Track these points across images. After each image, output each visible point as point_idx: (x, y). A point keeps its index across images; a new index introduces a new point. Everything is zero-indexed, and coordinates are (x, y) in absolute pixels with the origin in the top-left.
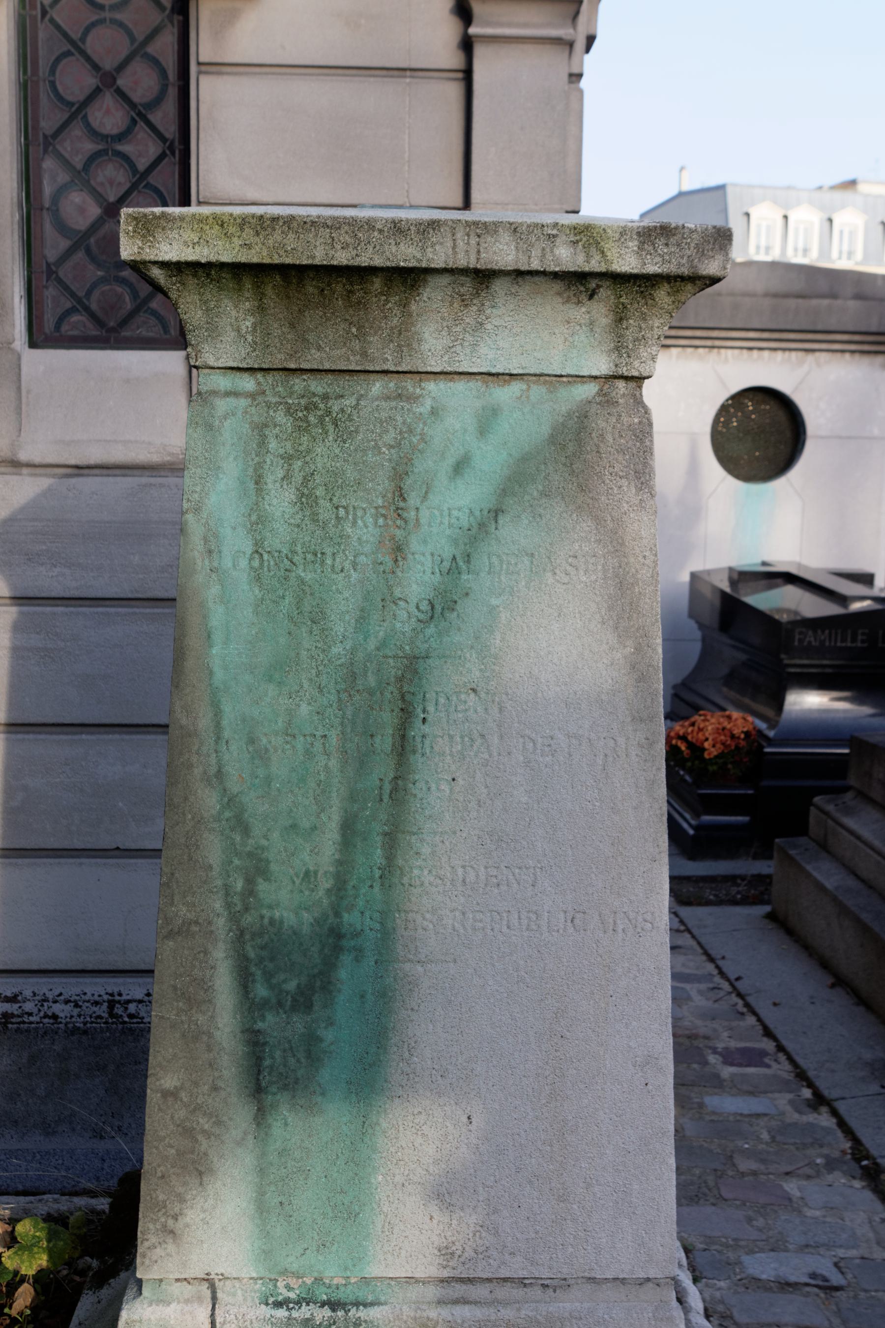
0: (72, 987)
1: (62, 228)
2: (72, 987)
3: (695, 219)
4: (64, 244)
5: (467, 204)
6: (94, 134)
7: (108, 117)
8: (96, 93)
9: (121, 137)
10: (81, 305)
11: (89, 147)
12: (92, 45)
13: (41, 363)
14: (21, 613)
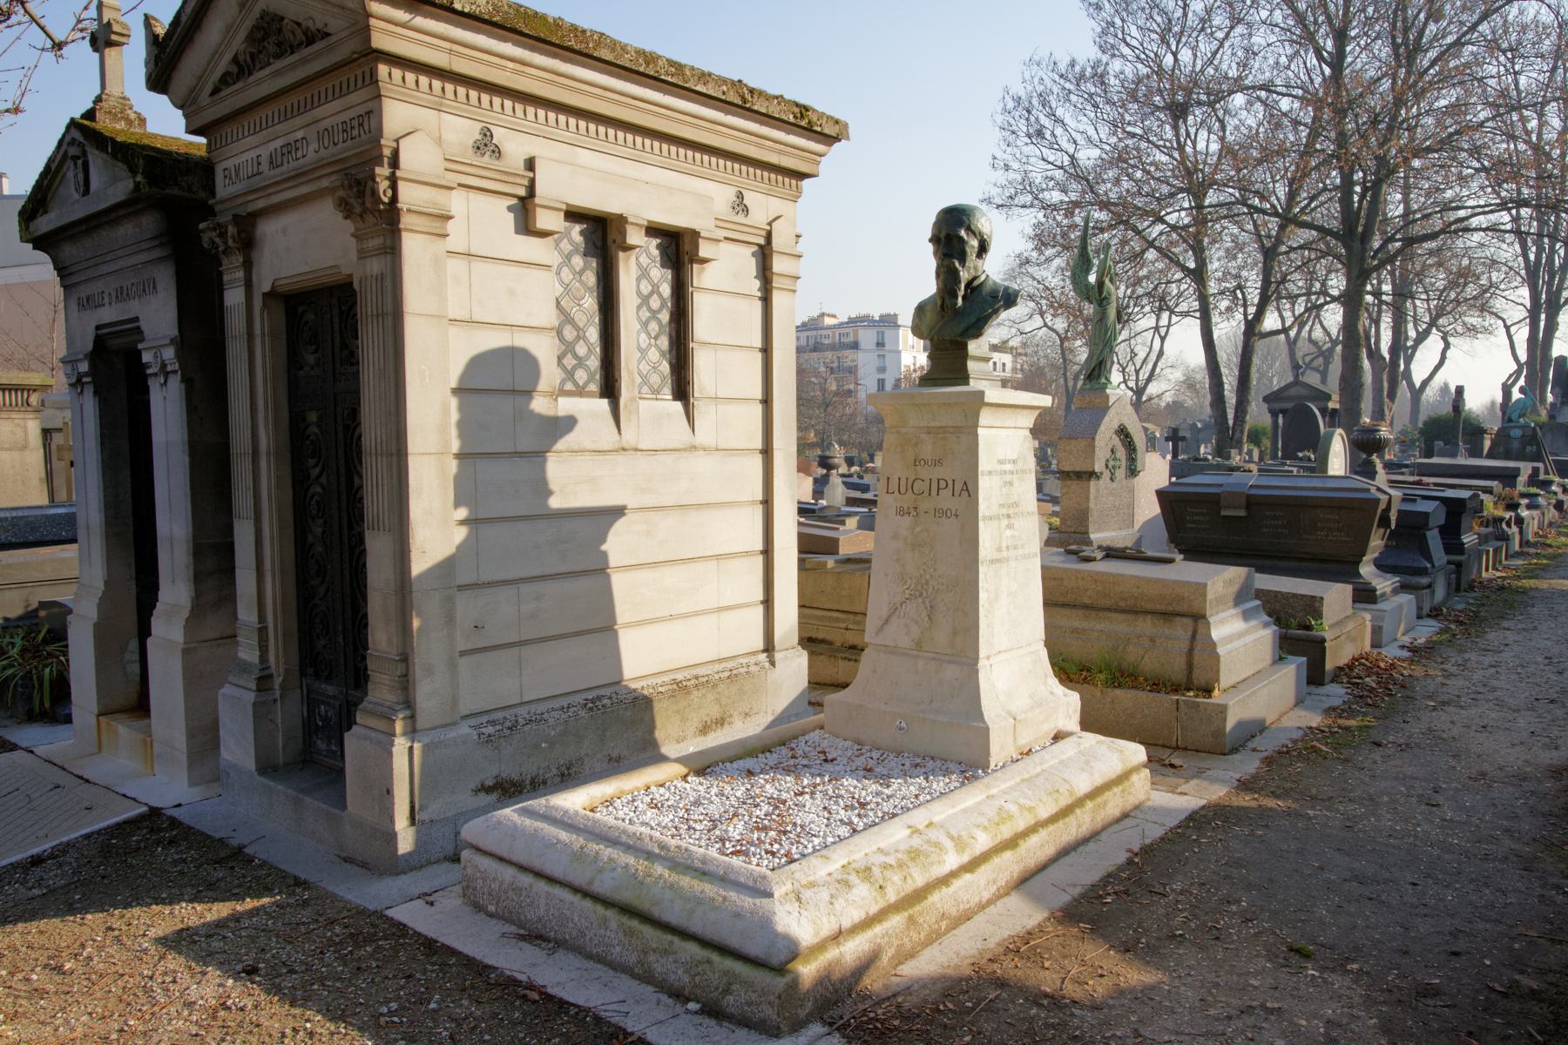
0: (718, 667)
2: (718, 667)
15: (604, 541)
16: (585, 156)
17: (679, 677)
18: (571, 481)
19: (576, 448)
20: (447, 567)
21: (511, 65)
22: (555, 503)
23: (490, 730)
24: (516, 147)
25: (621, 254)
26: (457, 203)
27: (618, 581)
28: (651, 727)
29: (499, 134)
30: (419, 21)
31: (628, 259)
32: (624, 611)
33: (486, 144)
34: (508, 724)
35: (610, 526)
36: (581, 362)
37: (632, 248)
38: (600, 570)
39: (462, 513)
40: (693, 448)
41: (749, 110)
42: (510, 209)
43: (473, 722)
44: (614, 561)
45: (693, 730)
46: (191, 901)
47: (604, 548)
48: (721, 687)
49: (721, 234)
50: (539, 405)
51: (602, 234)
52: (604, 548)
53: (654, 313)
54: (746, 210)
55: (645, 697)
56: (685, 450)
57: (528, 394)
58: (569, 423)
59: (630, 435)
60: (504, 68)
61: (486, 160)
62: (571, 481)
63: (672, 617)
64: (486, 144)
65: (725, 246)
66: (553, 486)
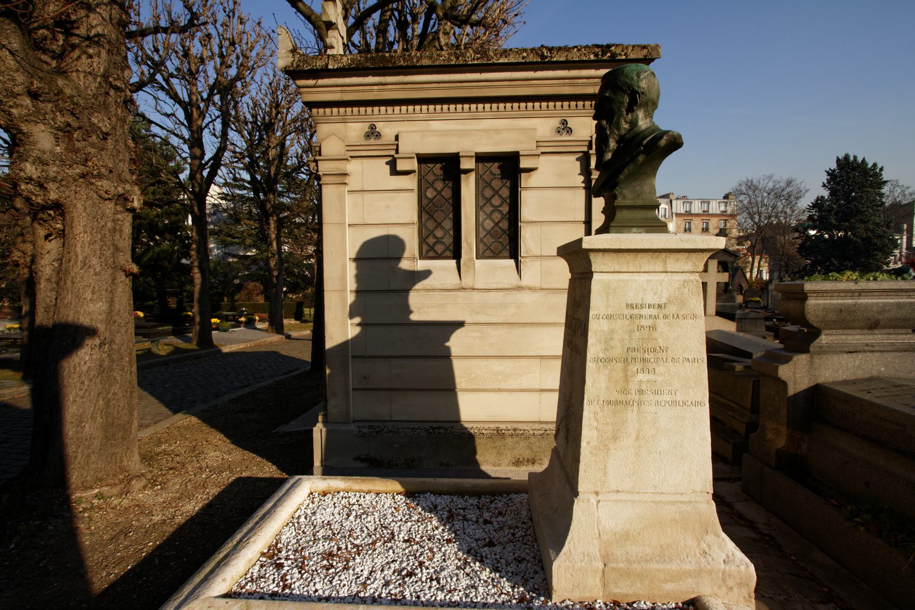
0: (537, 426)
1: (484, 229)
2: (537, 426)
3: (140, 338)
4: (485, 233)
5: (414, 171)
6: (493, 206)
7: (496, 201)
8: (494, 195)
9: (500, 206)
10: (488, 248)
11: (491, 209)
12: (493, 184)
13: (479, 263)
14: (24, 411)
15: (448, 340)
16: (436, 125)
17: (503, 426)
18: (424, 306)
19: (429, 287)
20: (344, 346)
21: (376, 87)
22: (414, 317)
23: (366, 430)
24: (388, 131)
25: (463, 176)
26: (353, 167)
27: (457, 365)
28: (474, 452)
29: (380, 126)
30: (321, 82)
31: (467, 178)
32: (461, 381)
33: (373, 133)
34: (378, 430)
35: (453, 332)
36: (439, 241)
37: (886, 182)
38: (446, 357)
39: (357, 320)
40: (519, 288)
41: (550, 62)
42: (387, 163)
43: (361, 424)
44: (455, 351)
45: (507, 461)
46: (555, 451)
47: (447, 344)
48: (533, 440)
49: (539, 151)
50: (405, 265)
51: (446, 167)
52: (447, 344)
53: (496, 209)
54: (570, 131)
55: (470, 434)
56: (513, 289)
57: (399, 259)
58: (427, 274)
59: (467, 281)
60: (372, 91)
61: (372, 141)
62: (424, 306)
63: (499, 390)
64: (373, 133)
65: (542, 158)
66: (412, 308)
